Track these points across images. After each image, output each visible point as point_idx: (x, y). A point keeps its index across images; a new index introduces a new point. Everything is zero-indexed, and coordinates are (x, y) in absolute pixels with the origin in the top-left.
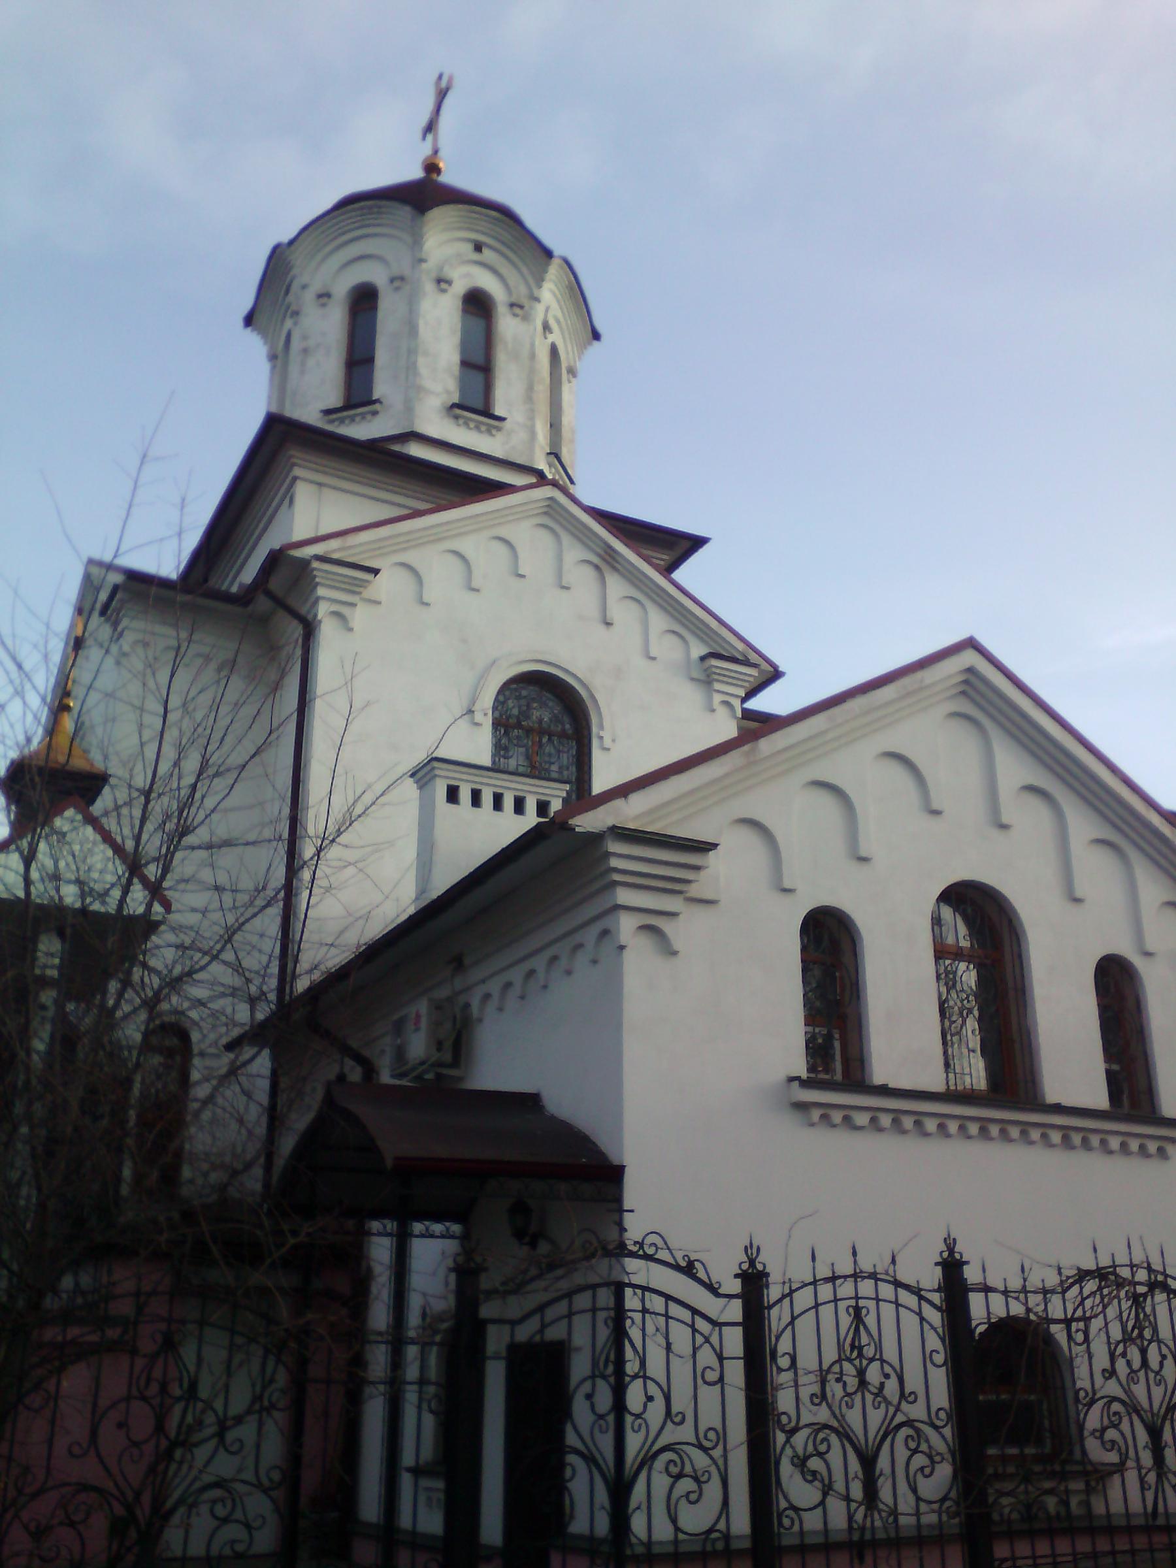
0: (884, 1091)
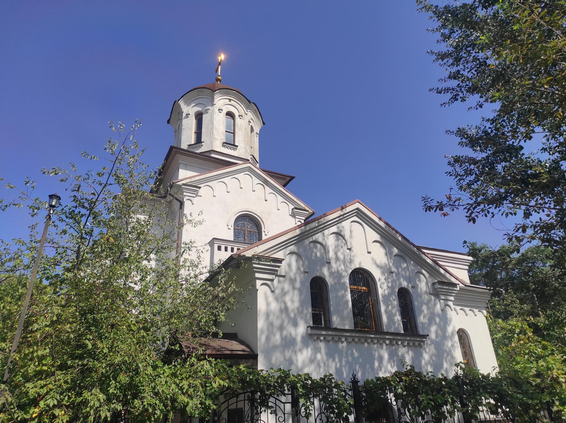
0: (336, 329)
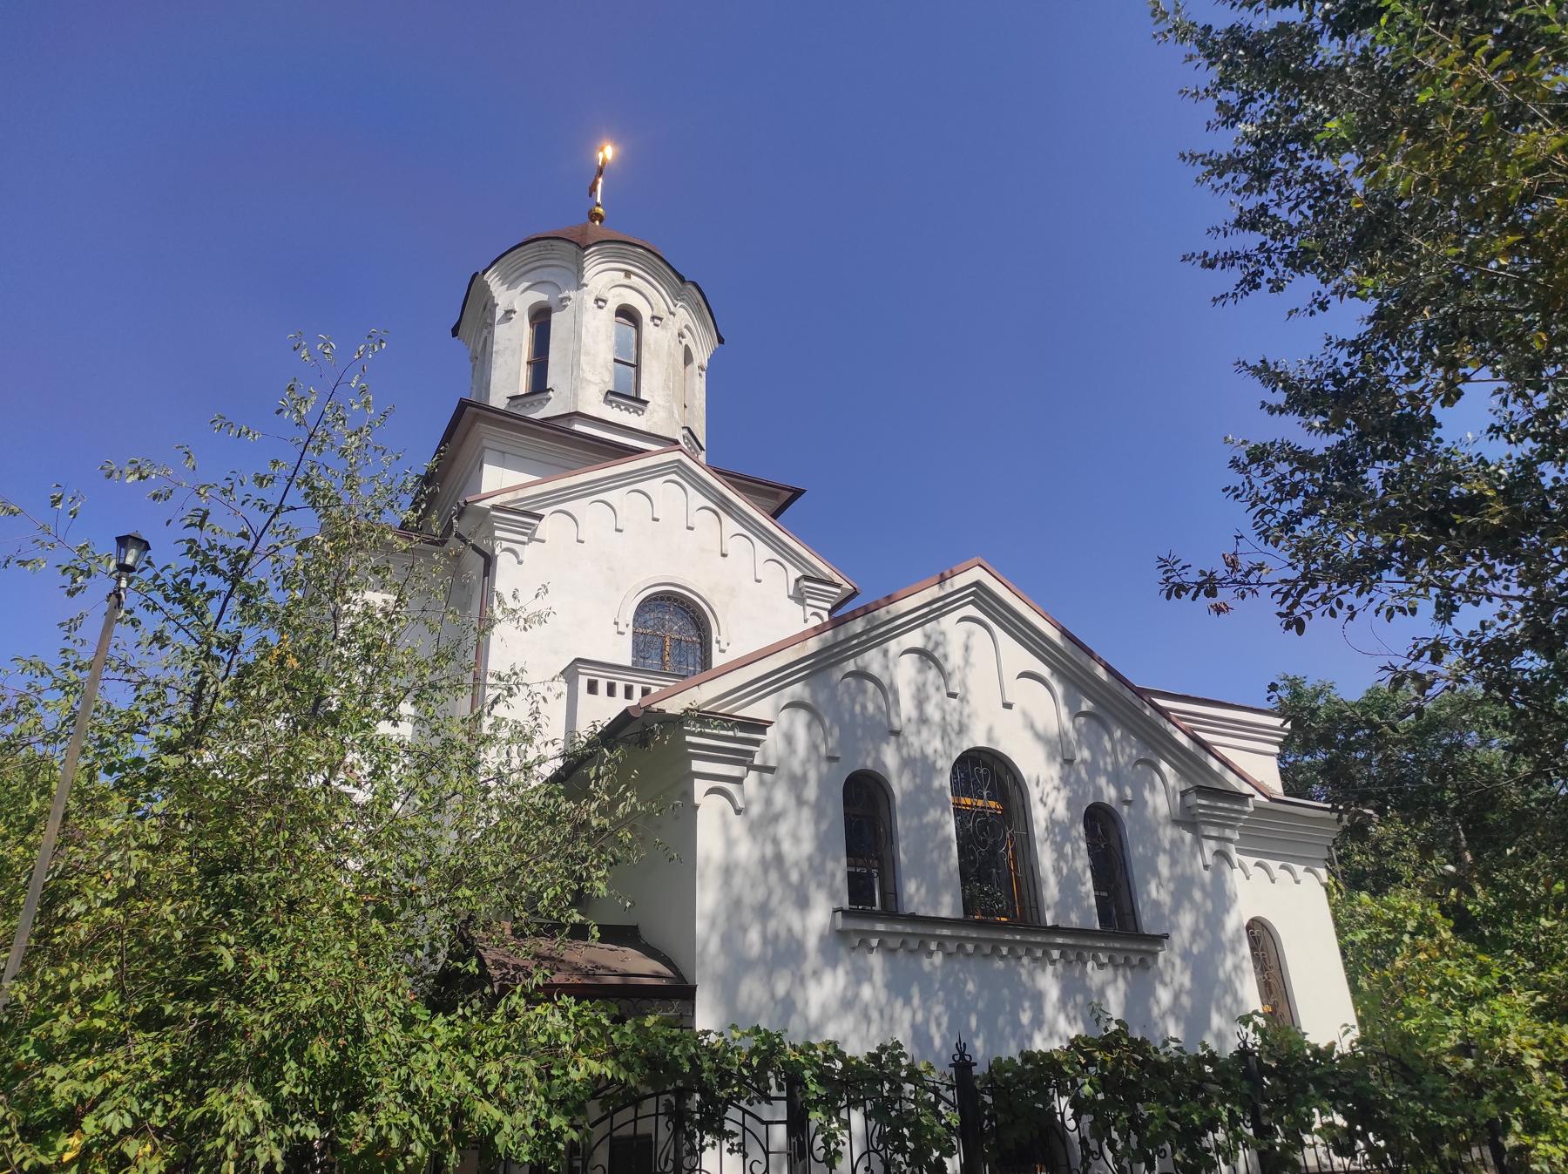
0: (913, 918)
